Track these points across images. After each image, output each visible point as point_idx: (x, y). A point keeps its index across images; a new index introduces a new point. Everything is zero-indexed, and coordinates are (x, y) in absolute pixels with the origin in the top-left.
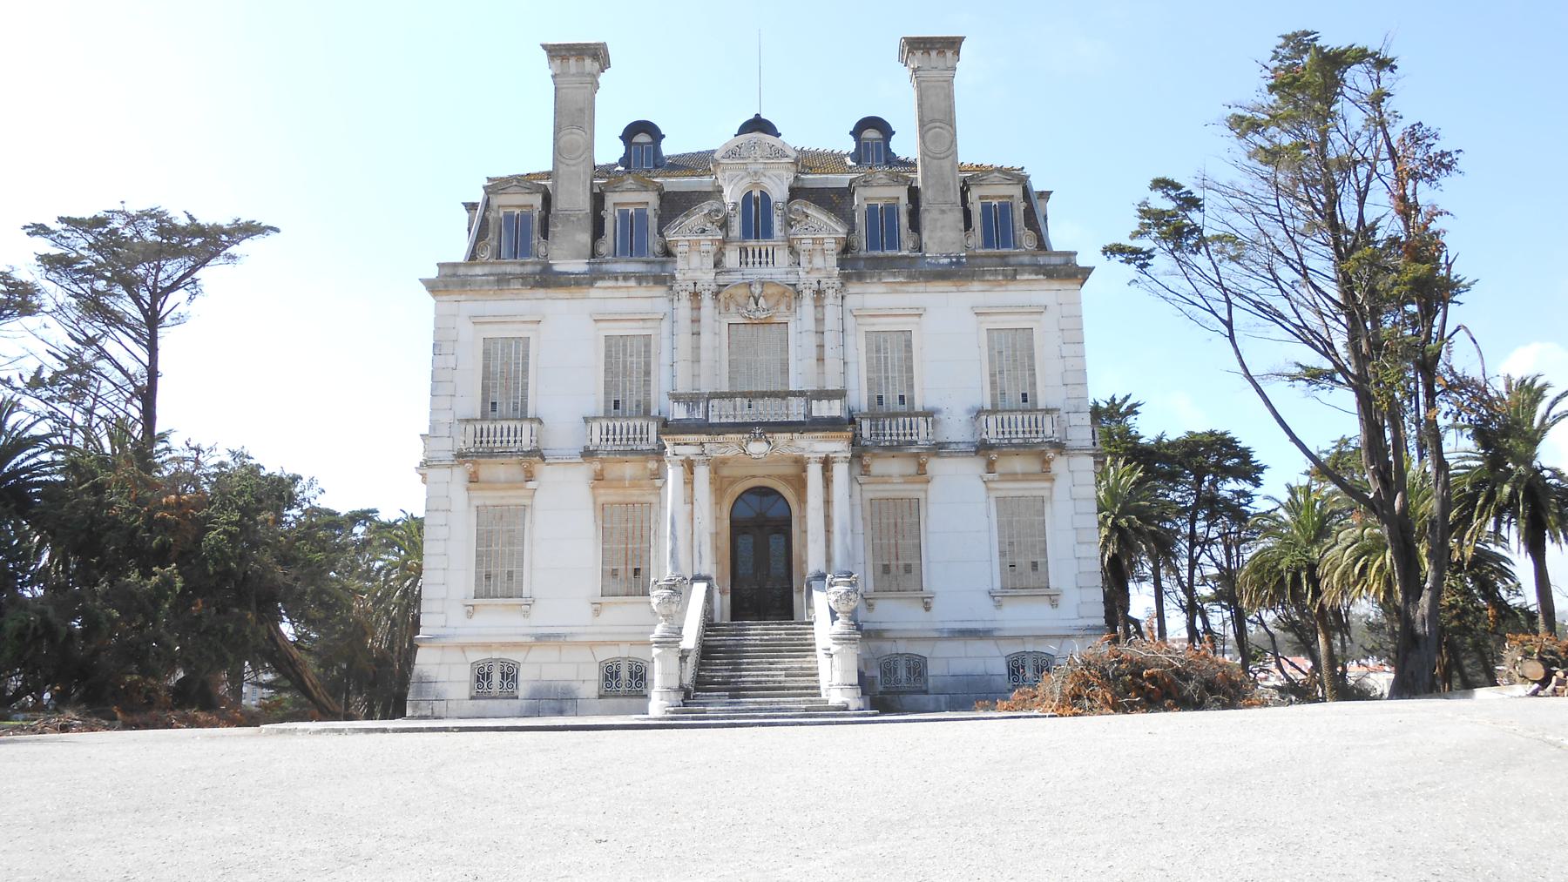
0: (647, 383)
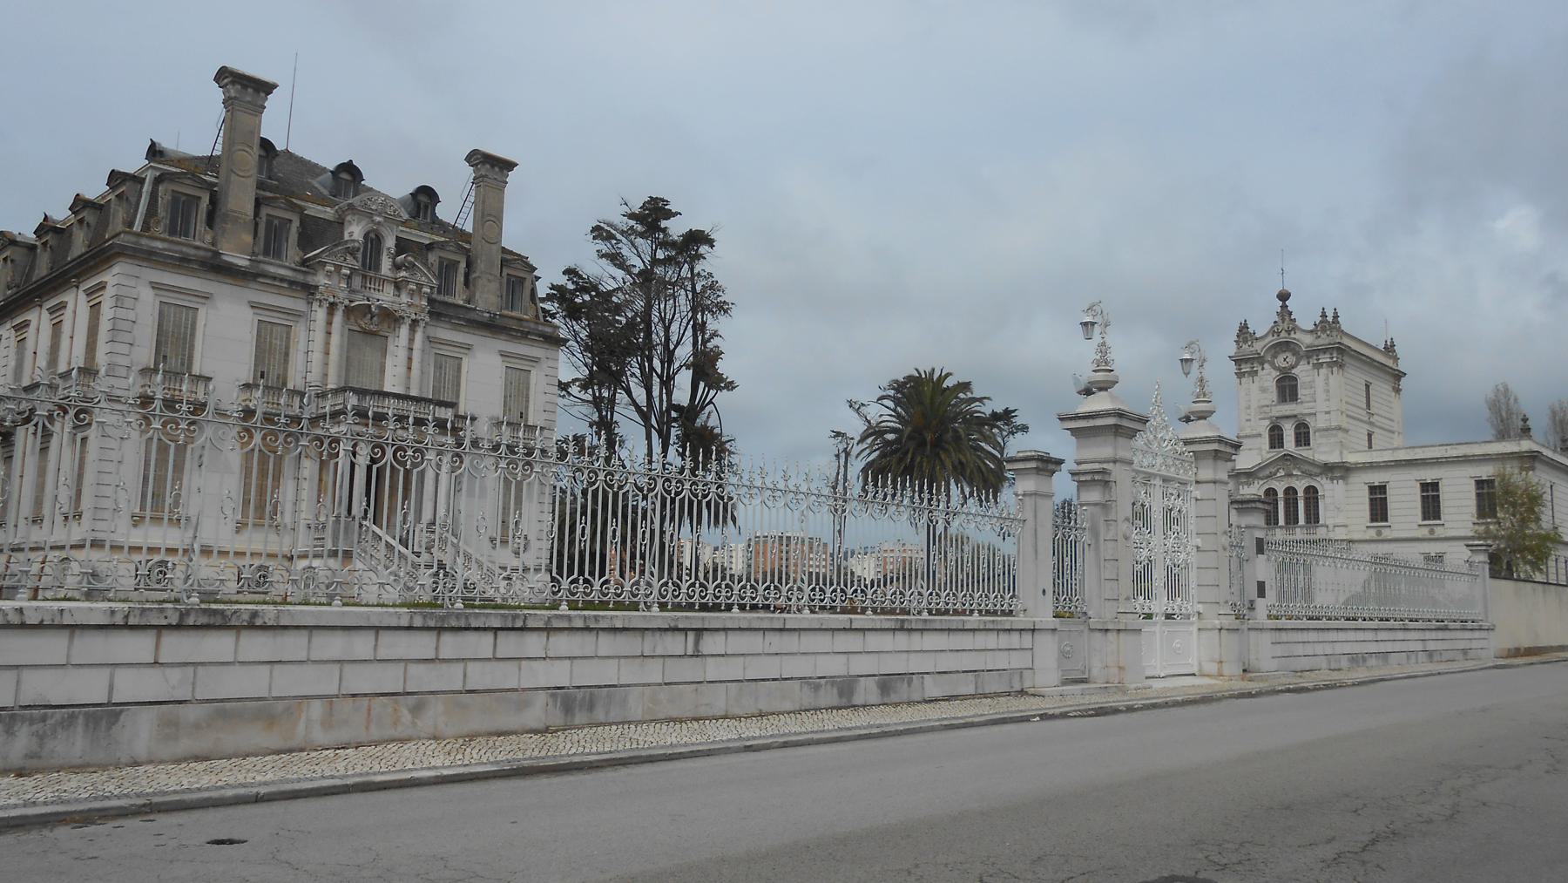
0: (286, 361)
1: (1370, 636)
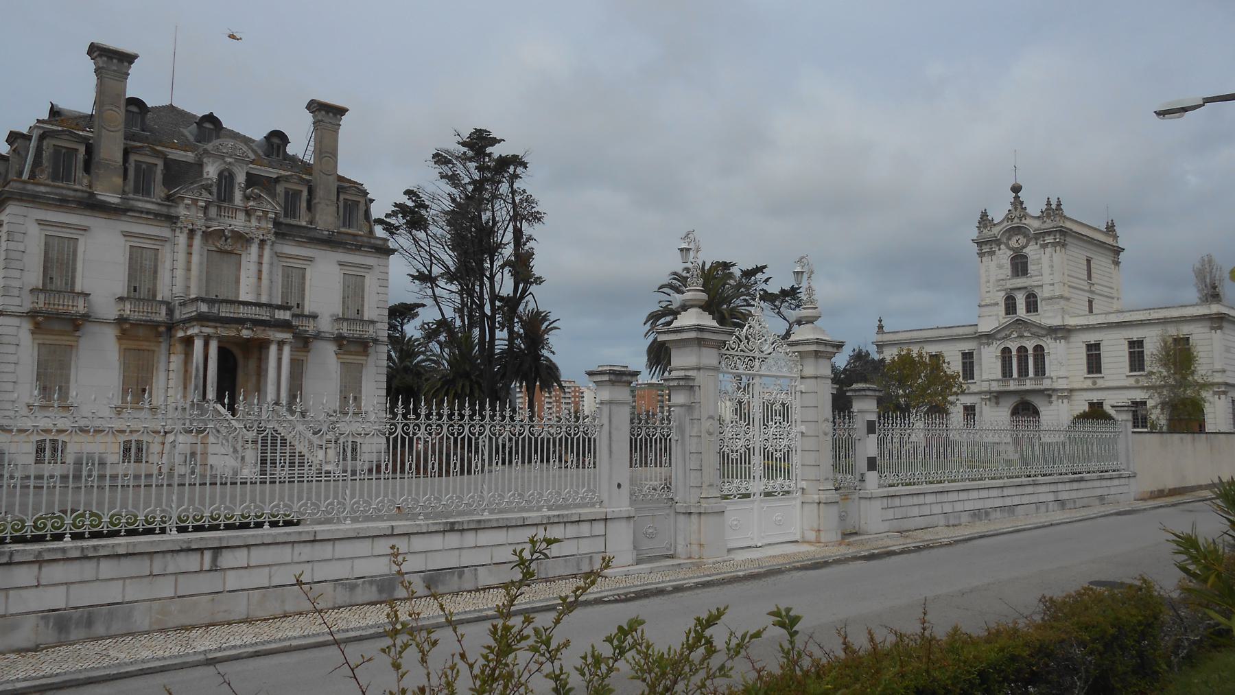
0: (155, 278)
1: (994, 493)
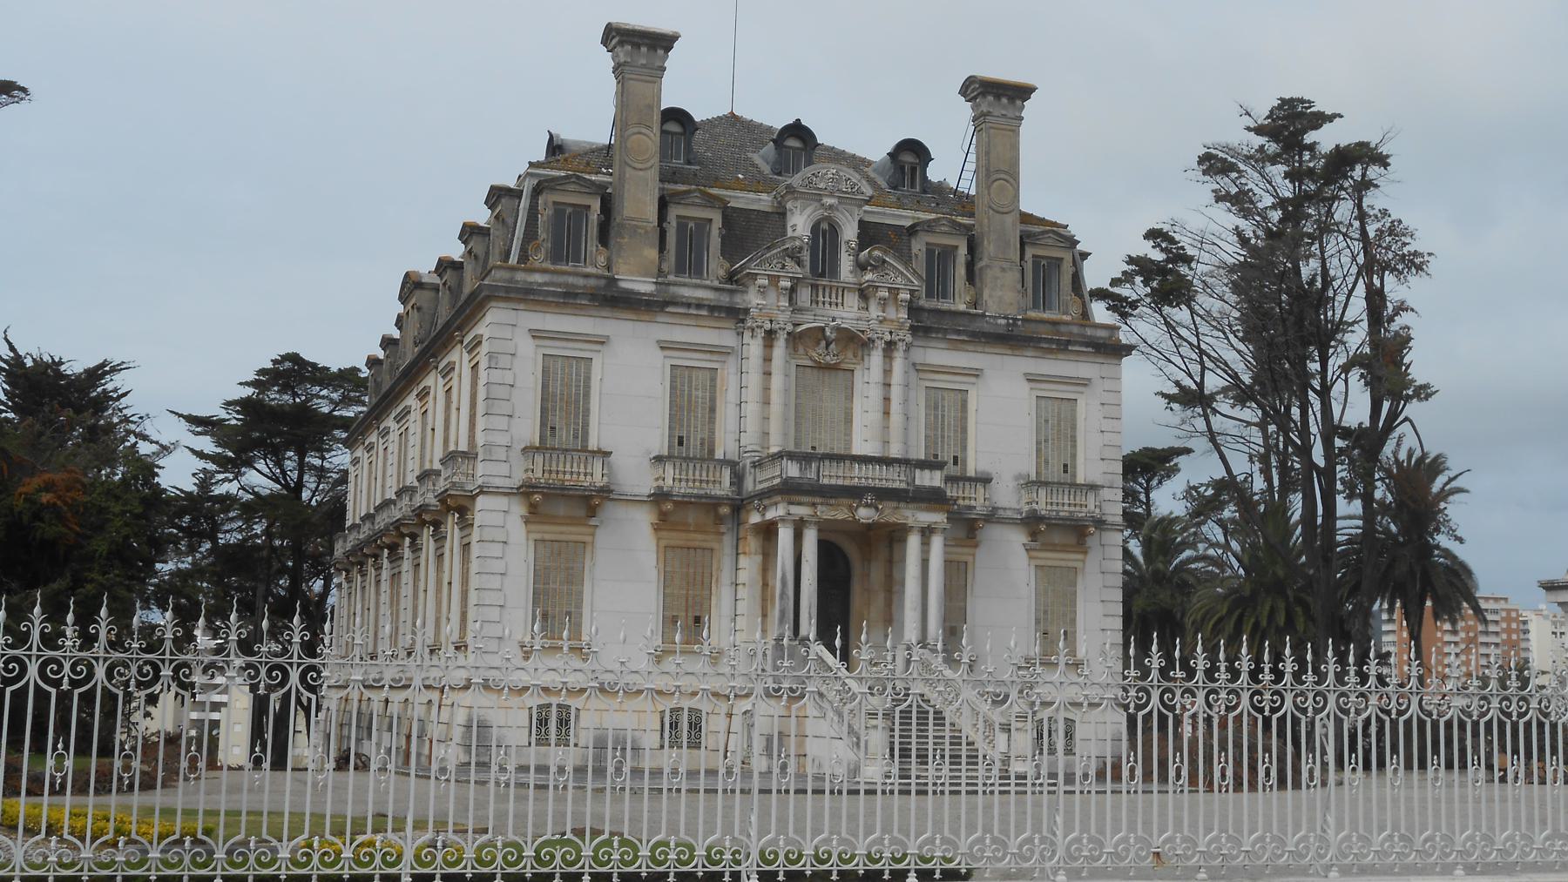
0: (712, 420)
